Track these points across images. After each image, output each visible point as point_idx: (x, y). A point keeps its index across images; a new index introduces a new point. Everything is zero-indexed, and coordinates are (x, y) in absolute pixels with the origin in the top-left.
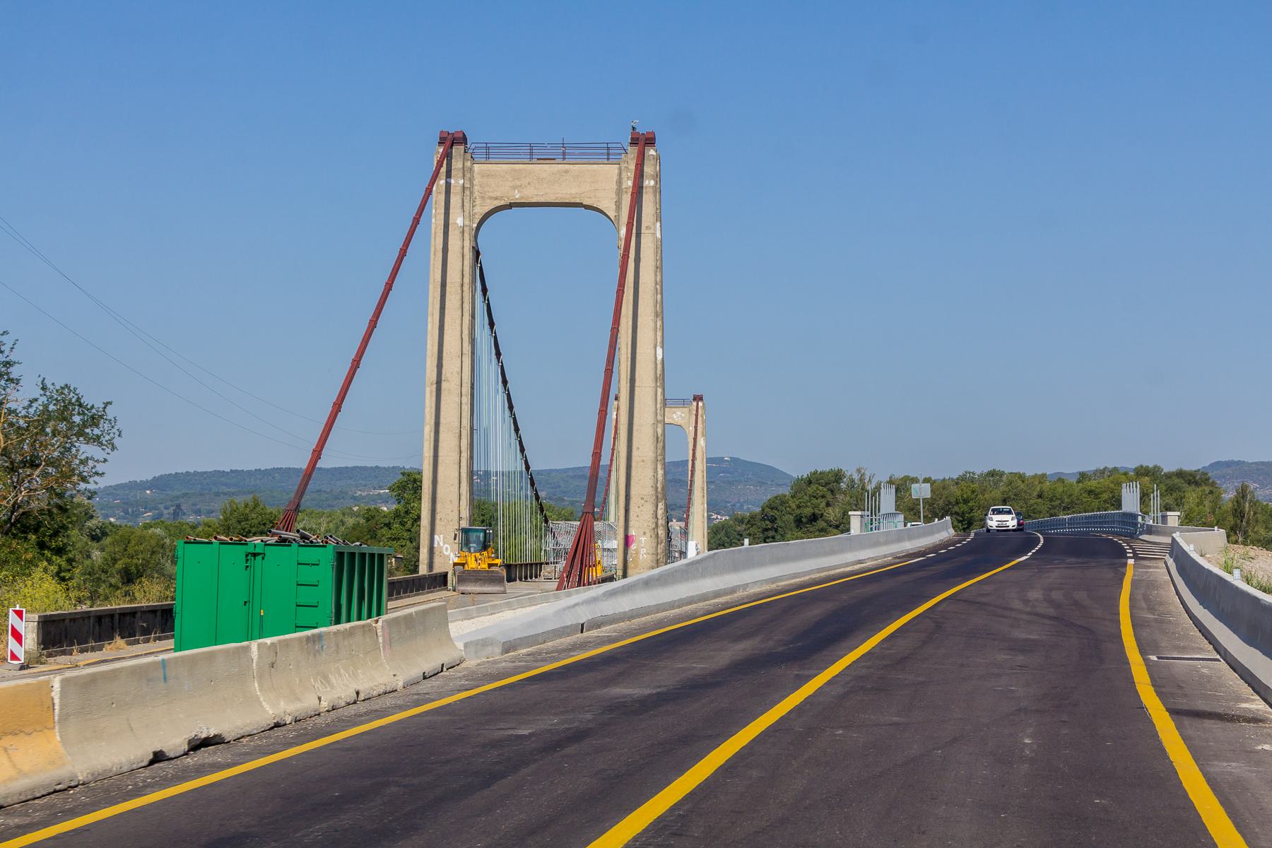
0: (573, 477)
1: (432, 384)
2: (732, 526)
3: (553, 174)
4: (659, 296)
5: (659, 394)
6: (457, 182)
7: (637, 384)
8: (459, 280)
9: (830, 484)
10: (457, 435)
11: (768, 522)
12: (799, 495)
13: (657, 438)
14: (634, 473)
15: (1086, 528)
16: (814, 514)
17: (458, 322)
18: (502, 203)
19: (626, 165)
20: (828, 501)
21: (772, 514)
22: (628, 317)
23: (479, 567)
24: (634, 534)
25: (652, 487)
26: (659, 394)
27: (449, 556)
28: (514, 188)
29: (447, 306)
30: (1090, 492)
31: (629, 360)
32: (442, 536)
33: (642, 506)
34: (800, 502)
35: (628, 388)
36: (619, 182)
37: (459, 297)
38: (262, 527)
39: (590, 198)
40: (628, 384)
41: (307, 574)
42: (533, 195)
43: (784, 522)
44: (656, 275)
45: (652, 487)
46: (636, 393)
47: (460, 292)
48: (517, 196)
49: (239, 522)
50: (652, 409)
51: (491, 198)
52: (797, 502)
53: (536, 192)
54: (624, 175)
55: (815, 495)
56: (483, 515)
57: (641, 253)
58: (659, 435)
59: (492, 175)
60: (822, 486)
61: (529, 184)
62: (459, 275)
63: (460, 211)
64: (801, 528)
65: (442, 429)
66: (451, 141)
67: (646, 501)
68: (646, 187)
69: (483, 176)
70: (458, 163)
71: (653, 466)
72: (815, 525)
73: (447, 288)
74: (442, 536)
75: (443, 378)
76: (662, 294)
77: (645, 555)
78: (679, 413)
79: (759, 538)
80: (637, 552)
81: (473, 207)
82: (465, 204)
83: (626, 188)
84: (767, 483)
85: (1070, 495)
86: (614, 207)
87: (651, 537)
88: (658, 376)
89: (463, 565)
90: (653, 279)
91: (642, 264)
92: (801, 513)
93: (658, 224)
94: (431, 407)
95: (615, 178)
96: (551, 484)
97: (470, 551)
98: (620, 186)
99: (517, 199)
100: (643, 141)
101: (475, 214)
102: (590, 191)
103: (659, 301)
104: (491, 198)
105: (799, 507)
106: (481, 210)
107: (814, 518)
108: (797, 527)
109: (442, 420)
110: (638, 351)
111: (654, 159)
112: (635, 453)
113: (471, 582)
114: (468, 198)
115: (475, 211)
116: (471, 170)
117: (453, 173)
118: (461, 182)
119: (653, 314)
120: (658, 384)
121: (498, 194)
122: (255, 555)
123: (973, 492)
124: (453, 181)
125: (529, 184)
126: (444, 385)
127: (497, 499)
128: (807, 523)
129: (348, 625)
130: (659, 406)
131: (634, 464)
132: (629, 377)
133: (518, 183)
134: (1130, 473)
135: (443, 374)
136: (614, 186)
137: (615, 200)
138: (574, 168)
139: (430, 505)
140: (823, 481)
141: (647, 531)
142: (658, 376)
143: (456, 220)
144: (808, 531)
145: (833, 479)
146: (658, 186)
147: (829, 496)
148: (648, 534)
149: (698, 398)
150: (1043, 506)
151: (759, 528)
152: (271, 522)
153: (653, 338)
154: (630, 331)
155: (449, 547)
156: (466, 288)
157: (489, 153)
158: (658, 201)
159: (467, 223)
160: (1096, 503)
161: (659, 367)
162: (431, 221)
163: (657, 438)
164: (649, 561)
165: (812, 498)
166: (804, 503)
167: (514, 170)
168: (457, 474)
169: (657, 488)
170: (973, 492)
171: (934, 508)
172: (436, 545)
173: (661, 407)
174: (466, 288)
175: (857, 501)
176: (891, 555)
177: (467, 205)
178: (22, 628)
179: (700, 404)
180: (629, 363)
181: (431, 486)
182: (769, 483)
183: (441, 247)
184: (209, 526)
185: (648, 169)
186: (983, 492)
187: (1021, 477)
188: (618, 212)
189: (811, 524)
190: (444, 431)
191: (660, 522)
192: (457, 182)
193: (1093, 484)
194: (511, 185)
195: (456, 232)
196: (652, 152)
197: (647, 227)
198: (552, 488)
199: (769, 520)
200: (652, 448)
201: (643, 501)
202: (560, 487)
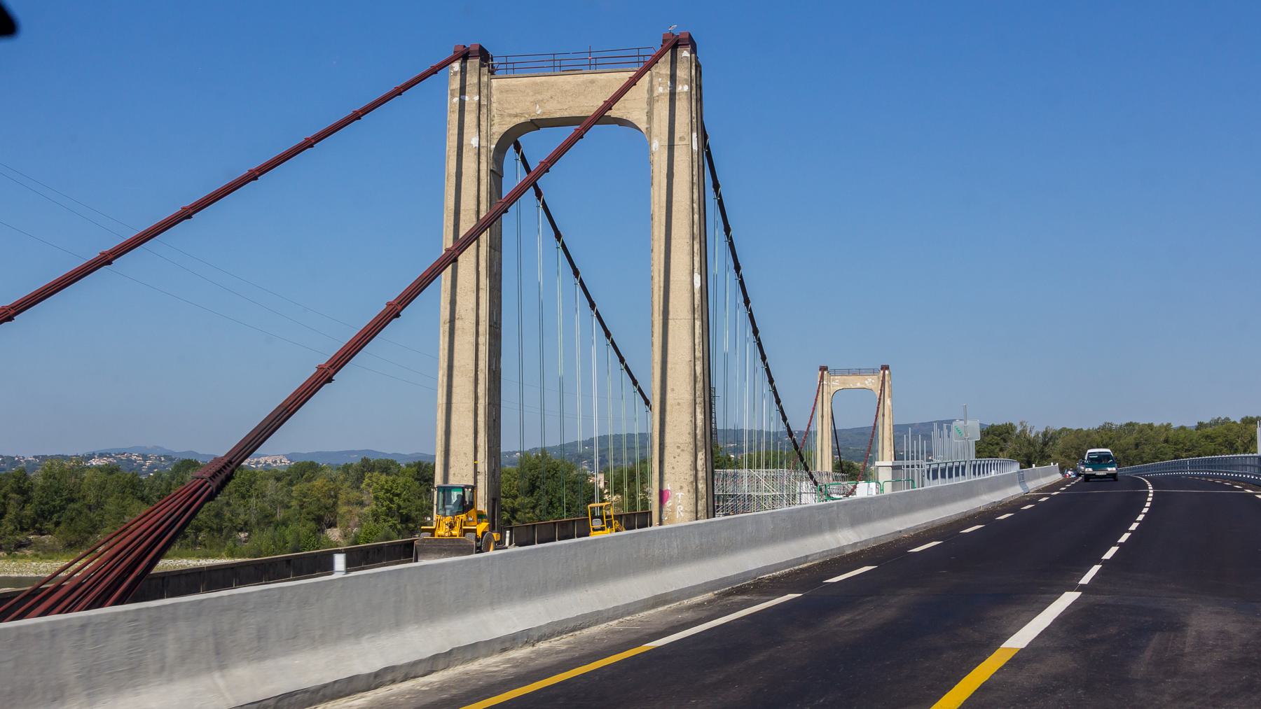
6: (471, 98)
7: (671, 316)
10: (472, 379)
14: (668, 418)
15: (1227, 473)
22: (659, 242)
24: (669, 488)
25: (689, 434)
28: (535, 103)
30: (1207, 437)
31: (662, 289)
40: (661, 317)
45: (689, 434)
46: (670, 327)
48: (539, 112)
49: (530, 470)
50: (689, 344)
51: (510, 115)
53: (559, 106)
57: (675, 168)
59: (512, 90)
61: (552, 98)
63: (475, 130)
65: (455, 373)
67: (683, 450)
68: (679, 93)
73: (461, 215)
75: (457, 317)
77: (681, 513)
78: (870, 380)
80: (673, 510)
82: (481, 123)
83: (658, 96)
85: (1191, 440)
86: (645, 118)
87: (689, 492)
88: (696, 306)
91: (675, 179)
101: (494, 133)
104: (510, 115)
106: (499, 129)
109: (456, 363)
110: (671, 278)
111: (687, 61)
112: (670, 395)
113: (435, 553)
114: (486, 116)
116: (489, 85)
117: (468, 89)
120: (696, 316)
121: (518, 111)
123: (1111, 438)
124: (467, 98)
125: (552, 98)
126: (458, 324)
127: (235, 461)
131: (668, 408)
132: (661, 308)
133: (540, 97)
135: (457, 312)
137: (646, 111)
138: (602, 78)
140: (997, 433)
141: (684, 485)
147: (1002, 443)
148: (686, 489)
149: (885, 368)
150: (1169, 449)
152: (554, 469)
154: (663, 256)
160: (1212, 446)
161: (697, 296)
167: (536, 84)
168: (472, 424)
170: (1111, 438)
171: (1080, 452)
177: (483, 124)
179: (887, 372)
180: (662, 293)
181: (444, 437)
183: (455, 171)
184: (509, 474)
186: (1119, 438)
187: (1150, 426)
188: (650, 124)
190: (457, 375)
192: (471, 98)
193: (1209, 430)
195: (470, 154)
197: (680, 138)
201: (679, 451)
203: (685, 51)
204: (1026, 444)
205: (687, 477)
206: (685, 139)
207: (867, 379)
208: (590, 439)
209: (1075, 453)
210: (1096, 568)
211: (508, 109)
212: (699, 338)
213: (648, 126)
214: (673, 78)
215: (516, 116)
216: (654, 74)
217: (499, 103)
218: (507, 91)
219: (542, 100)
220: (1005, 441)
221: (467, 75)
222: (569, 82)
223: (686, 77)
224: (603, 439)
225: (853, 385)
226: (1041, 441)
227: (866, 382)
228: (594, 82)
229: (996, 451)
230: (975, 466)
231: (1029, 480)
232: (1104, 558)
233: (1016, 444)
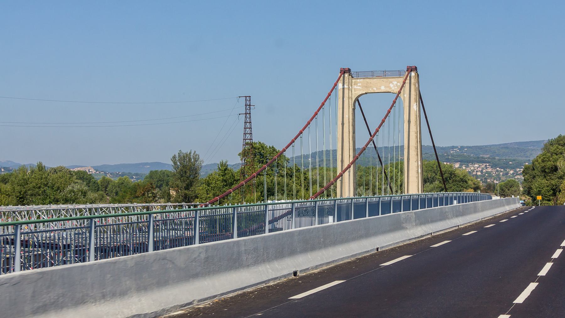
0: (502, 148)
34: (544, 158)
38: (37, 190)
72: (555, 174)
78: (395, 83)
96: (491, 151)
128: (549, 173)
129: (472, 202)
134: (129, 313)
140: (561, 142)
144: (550, 178)
149: (411, 69)
151: (531, 175)
165: (554, 154)
166: (547, 158)
189: (553, 173)
198: (492, 153)
202: (496, 153)
207: (391, 82)
208: (315, 152)
210: (532, 286)
224: (314, 155)
225: (377, 89)
227: (391, 85)
232: (540, 274)
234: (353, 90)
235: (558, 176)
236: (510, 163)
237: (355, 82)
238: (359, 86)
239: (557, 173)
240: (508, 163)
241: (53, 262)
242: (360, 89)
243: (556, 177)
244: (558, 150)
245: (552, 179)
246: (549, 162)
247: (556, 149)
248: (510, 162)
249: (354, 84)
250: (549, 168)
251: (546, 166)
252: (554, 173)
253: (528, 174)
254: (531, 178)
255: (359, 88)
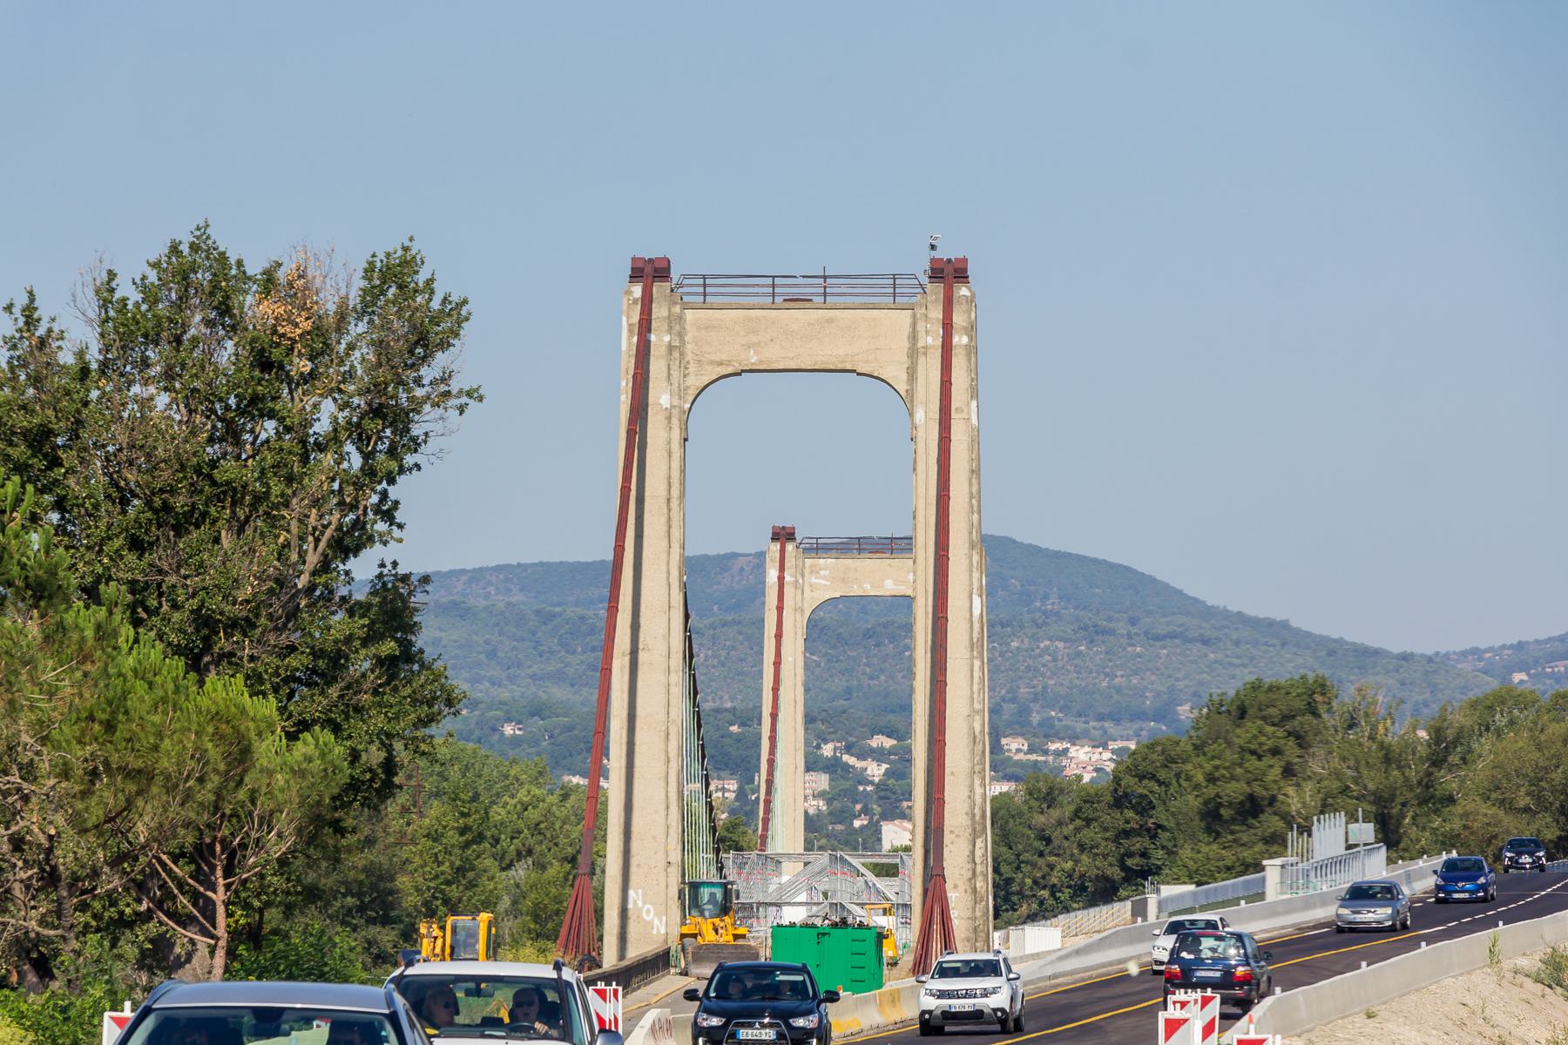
1: (623, 655)
2: (1021, 814)
3: (809, 324)
4: (976, 516)
5: (976, 668)
8: (665, 493)
9: (1293, 717)
10: (663, 735)
11: (1130, 814)
12: (1212, 749)
13: (975, 738)
16: (1251, 798)
17: (664, 557)
18: (730, 370)
19: (923, 310)
20: (1289, 763)
21: (1140, 790)
23: (721, 940)
25: (967, 814)
26: (976, 668)
27: (651, 922)
28: (748, 346)
29: (645, 534)
31: (930, 616)
32: (640, 891)
33: (952, 843)
34: (1216, 768)
35: (929, 660)
36: (913, 337)
37: (664, 519)
39: (867, 362)
41: (859, 947)
42: (776, 355)
43: (1173, 814)
44: (971, 484)
45: (967, 814)
47: (666, 511)
48: (753, 359)
51: (711, 363)
52: (1208, 767)
54: (921, 326)
55: (1253, 747)
56: (463, 815)
58: (977, 733)
60: (1274, 725)
61: (772, 340)
62: (664, 486)
64: (1218, 835)
66: (650, 272)
67: (957, 836)
69: (699, 328)
70: (662, 309)
71: (967, 783)
73: (646, 504)
74: (640, 891)
75: (641, 646)
76: (979, 512)
79: (1105, 856)
81: (685, 376)
82: (672, 372)
84: (1112, 632)
86: (905, 376)
87: (966, 891)
88: (975, 640)
89: (694, 936)
90: (967, 491)
92: (1217, 795)
93: (974, 404)
94: (623, 692)
95: (907, 330)
97: (702, 914)
98: (914, 345)
99: (753, 364)
100: (950, 273)
102: (868, 350)
103: (975, 523)
104: (711, 363)
105: (1211, 779)
106: (694, 382)
107: (1252, 808)
108: (1209, 830)
109: (640, 711)
111: (967, 302)
114: (677, 362)
115: (688, 383)
116: (681, 319)
118: (667, 338)
119: (967, 545)
121: (724, 357)
122: (824, 934)
124: (653, 338)
125: (772, 340)
126: (642, 656)
128: (1233, 820)
130: (976, 687)
132: (929, 643)
133: (755, 339)
135: (641, 640)
136: (905, 344)
137: (906, 366)
138: (843, 316)
139: (622, 844)
140: (1273, 711)
141: (960, 883)
142: (975, 640)
143: (660, 398)
145: (1300, 704)
146: (973, 344)
147: (1291, 749)
153: (967, 583)
155: (652, 909)
156: (675, 503)
157: (707, 288)
158: (973, 365)
159: (676, 402)
162: (619, 399)
163: (975, 738)
164: (964, 930)
165: (1247, 756)
167: (750, 319)
169: (974, 815)
172: (630, 906)
173: (979, 690)
174: (675, 503)
175: (1357, 769)
176: (1293, 925)
177: (675, 374)
178: (109, 1030)
181: (623, 814)
182: (1122, 627)
185: (959, 319)
191: (979, 869)
194: (743, 342)
196: (964, 291)
199: (1133, 807)
200: (967, 754)
203: (964, 288)
204: (1376, 756)
205: (964, 871)
206: (962, 411)
209: (1528, 794)
211: (709, 353)
212: (978, 684)
213: (909, 388)
214: (948, 326)
215: (720, 364)
216: (918, 316)
217: (696, 344)
218: (707, 328)
219: (759, 343)
220: (1300, 738)
221: (654, 305)
222: (797, 319)
223: (964, 324)
226: (1422, 751)
228: (832, 322)
229: (1270, 778)
230: (1316, 868)
231: (1416, 880)
233: (1344, 759)
234: (807, 589)
235: (1267, 834)
236: (509, 730)
237: (811, 566)
238: (824, 578)
239: (1259, 822)
240: (494, 729)
241: (1479, 882)
242: (825, 585)
243: (1255, 835)
244: (1265, 738)
245: (1243, 845)
246: (1234, 784)
247: (1255, 737)
248: (509, 720)
249: (811, 573)
250: (1230, 804)
251: (1220, 798)
252: (1252, 821)
253: (1096, 824)
254: (1106, 839)
255: (823, 582)
